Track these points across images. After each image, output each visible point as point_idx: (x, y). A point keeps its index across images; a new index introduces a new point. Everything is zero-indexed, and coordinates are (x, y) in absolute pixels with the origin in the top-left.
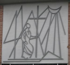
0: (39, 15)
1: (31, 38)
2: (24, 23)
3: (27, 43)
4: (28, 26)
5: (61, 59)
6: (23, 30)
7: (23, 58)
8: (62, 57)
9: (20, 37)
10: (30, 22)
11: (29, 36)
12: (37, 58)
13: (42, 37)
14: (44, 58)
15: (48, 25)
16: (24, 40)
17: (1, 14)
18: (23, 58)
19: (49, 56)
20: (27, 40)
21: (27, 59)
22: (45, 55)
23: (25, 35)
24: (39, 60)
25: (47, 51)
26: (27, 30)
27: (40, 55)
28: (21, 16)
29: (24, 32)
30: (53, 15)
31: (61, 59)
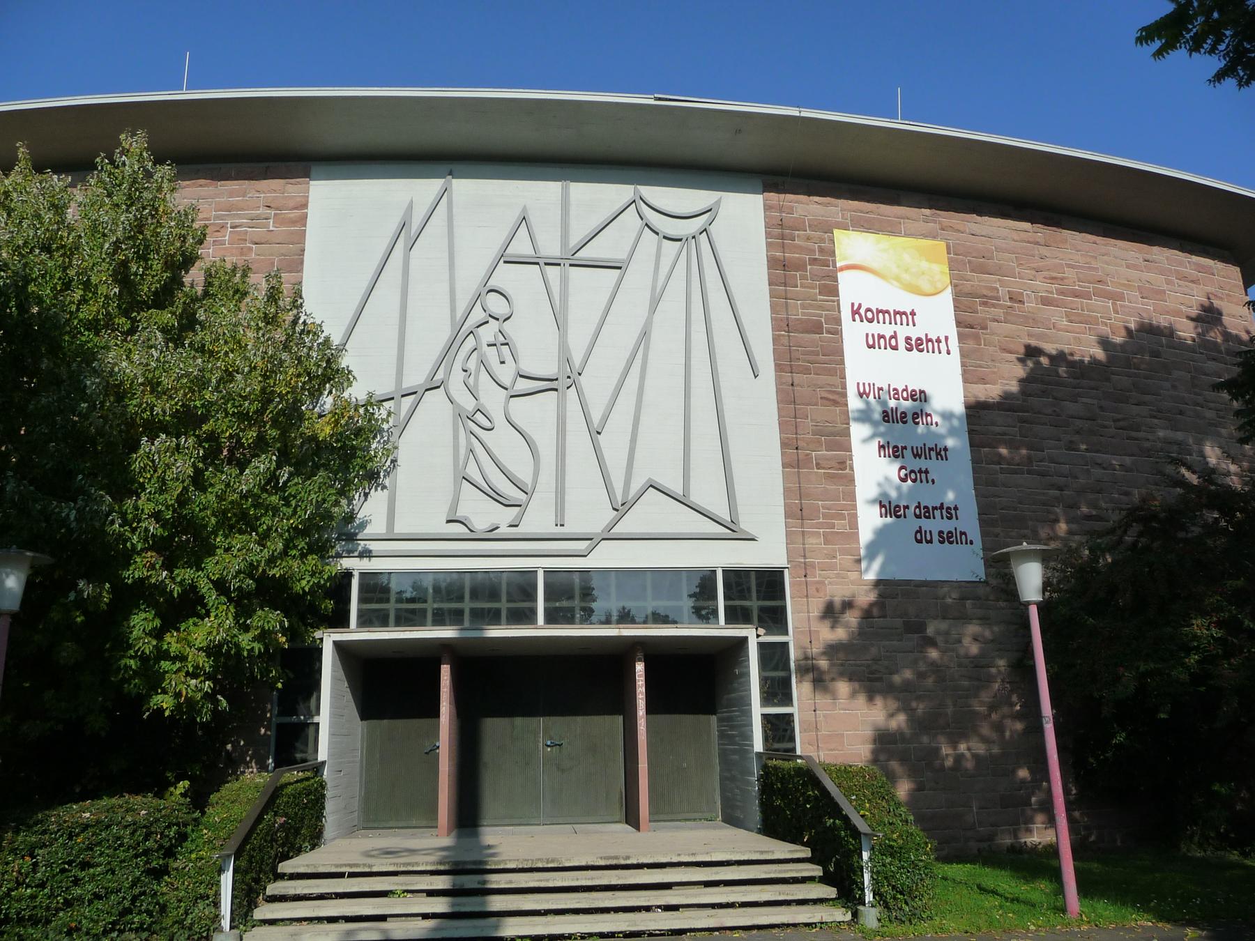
0: (574, 241)
1: (524, 385)
2: (468, 284)
3: (487, 424)
4: (496, 304)
5: (734, 532)
6: (460, 333)
7: (458, 529)
8: (746, 525)
9: (440, 376)
10: (506, 277)
11: (506, 374)
12: (567, 530)
13: (597, 385)
14: (619, 529)
15: (643, 310)
16: (469, 404)
17: (293, 222)
18: (458, 529)
19: (653, 514)
20: (493, 399)
21: (491, 535)
22: (622, 508)
23: (472, 364)
24: (582, 546)
25: (635, 487)
26: (488, 333)
27: (587, 512)
28: (459, 295)
29: (470, 343)
30: (670, 248)
31: (734, 532)
